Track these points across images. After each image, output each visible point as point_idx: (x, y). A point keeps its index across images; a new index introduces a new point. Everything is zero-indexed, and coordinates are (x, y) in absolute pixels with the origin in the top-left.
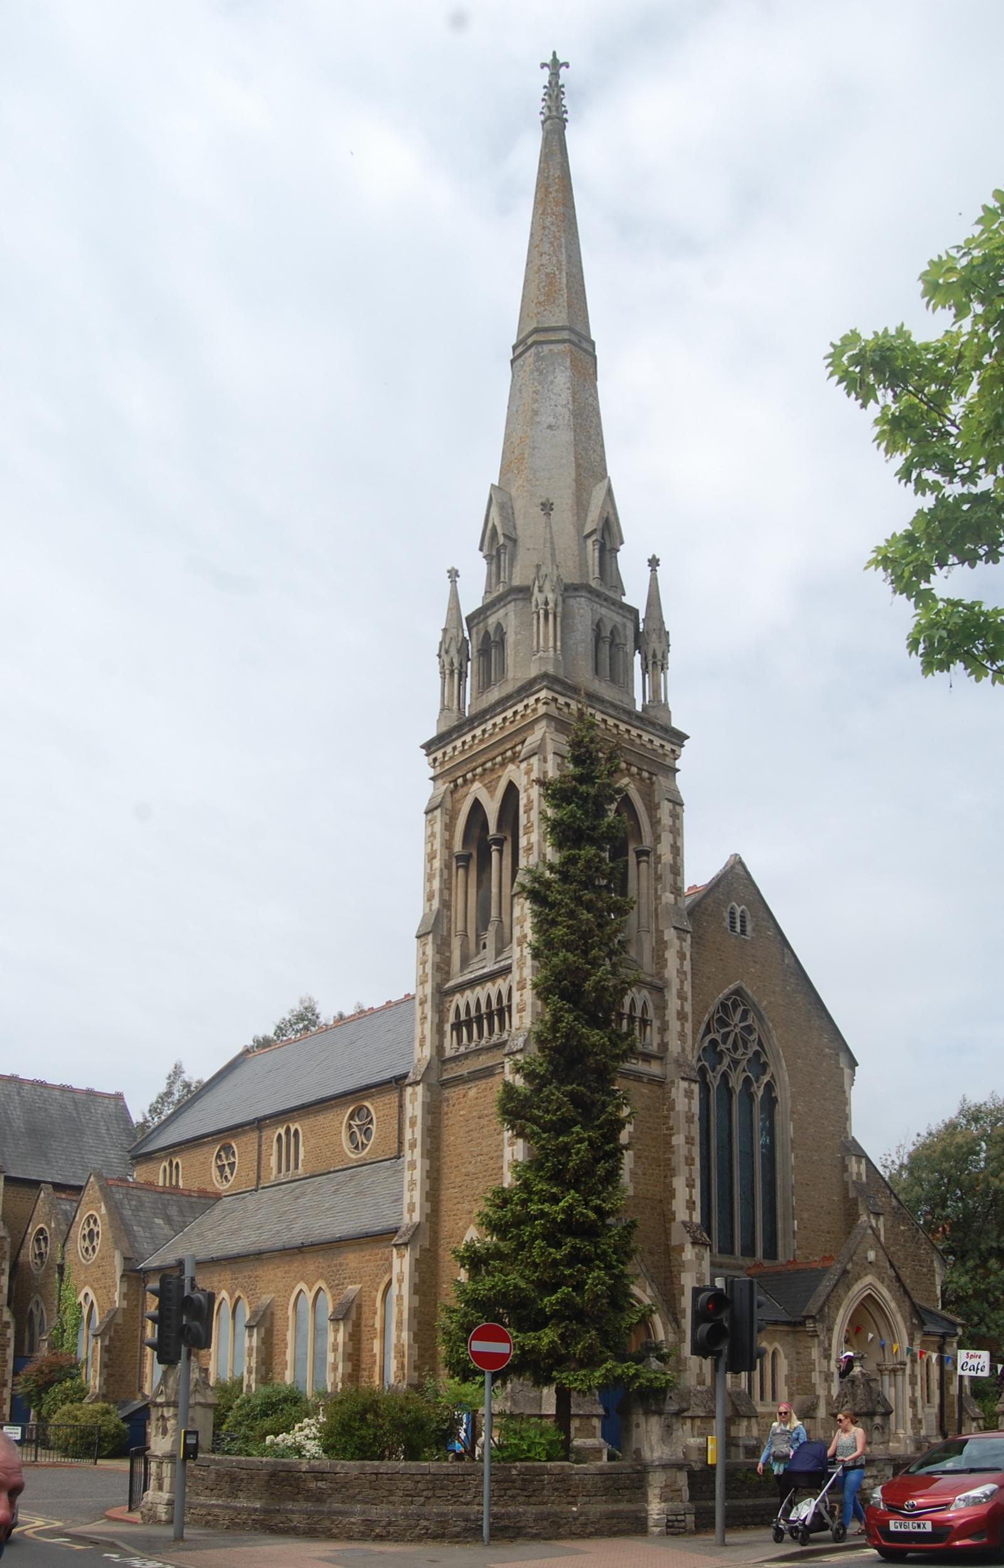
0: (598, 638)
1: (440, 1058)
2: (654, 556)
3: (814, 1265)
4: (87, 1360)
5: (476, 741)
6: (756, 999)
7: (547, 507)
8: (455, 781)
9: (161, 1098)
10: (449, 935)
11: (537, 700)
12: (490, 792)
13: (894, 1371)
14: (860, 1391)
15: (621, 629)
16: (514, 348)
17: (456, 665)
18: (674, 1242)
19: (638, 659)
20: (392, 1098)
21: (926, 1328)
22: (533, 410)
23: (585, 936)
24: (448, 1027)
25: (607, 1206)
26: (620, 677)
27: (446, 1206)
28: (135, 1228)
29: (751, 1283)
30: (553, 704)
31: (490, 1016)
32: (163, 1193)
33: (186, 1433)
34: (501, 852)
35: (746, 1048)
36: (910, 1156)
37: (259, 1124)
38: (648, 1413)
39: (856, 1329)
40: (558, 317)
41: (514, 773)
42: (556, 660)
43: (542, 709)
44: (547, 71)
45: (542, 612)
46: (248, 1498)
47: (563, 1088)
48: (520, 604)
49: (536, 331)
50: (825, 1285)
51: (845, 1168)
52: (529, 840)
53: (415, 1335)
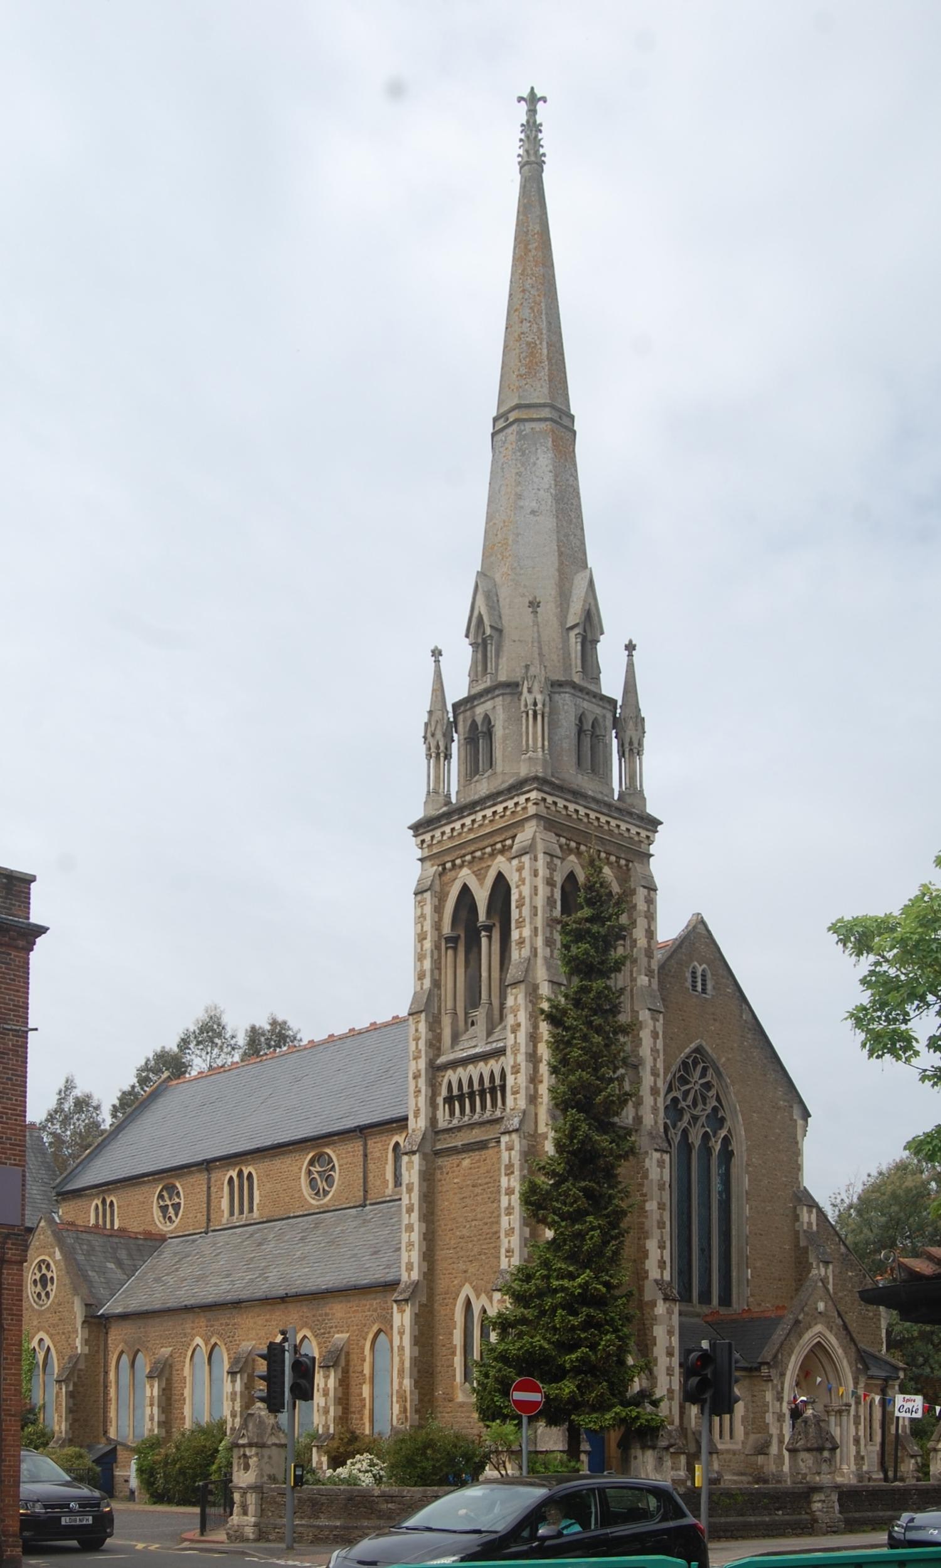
0: (580, 731)
1: (434, 1130)
2: (631, 641)
3: (768, 1314)
4: (44, 1406)
5: (465, 830)
6: (714, 1056)
7: (534, 605)
8: (444, 864)
9: (50, 1115)
10: (440, 1013)
11: (527, 800)
12: (479, 880)
13: (840, 1412)
14: (812, 1430)
15: (601, 720)
16: (495, 420)
17: (442, 748)
18: (647, 1297)
19: (615, 742)
20: (356, 1146)
21: (870, 1373)
22: (516, 494)
23: (595, 1056)
24: (440, 1100)
25: (615, 1282)
26: (598, 767)
27: (441, 1266)
28: (90, 1273)
29: (730, 1344)
30: (542, 804)
31: (482, 1093)
32: (111, 1236)
33: (295, 1466)
34: (490, 938)
35: (705, 1104)
36: (859, 1198)
37: (207, 1165)
38: (644, 1447)
39: (806, 1374)
40: (539, 393)
41: (500, 863)
42: (545, 760)
43: (532, 810)
44: (524, 106)
45: (531, 712)
46: (329, 1518)
47: (577, 1185)
48: (508, 698)
49: (518, 407)
50: (779, 1334)
51: (797, 1218)
52: (521, 934)
53: (416, 1382)
